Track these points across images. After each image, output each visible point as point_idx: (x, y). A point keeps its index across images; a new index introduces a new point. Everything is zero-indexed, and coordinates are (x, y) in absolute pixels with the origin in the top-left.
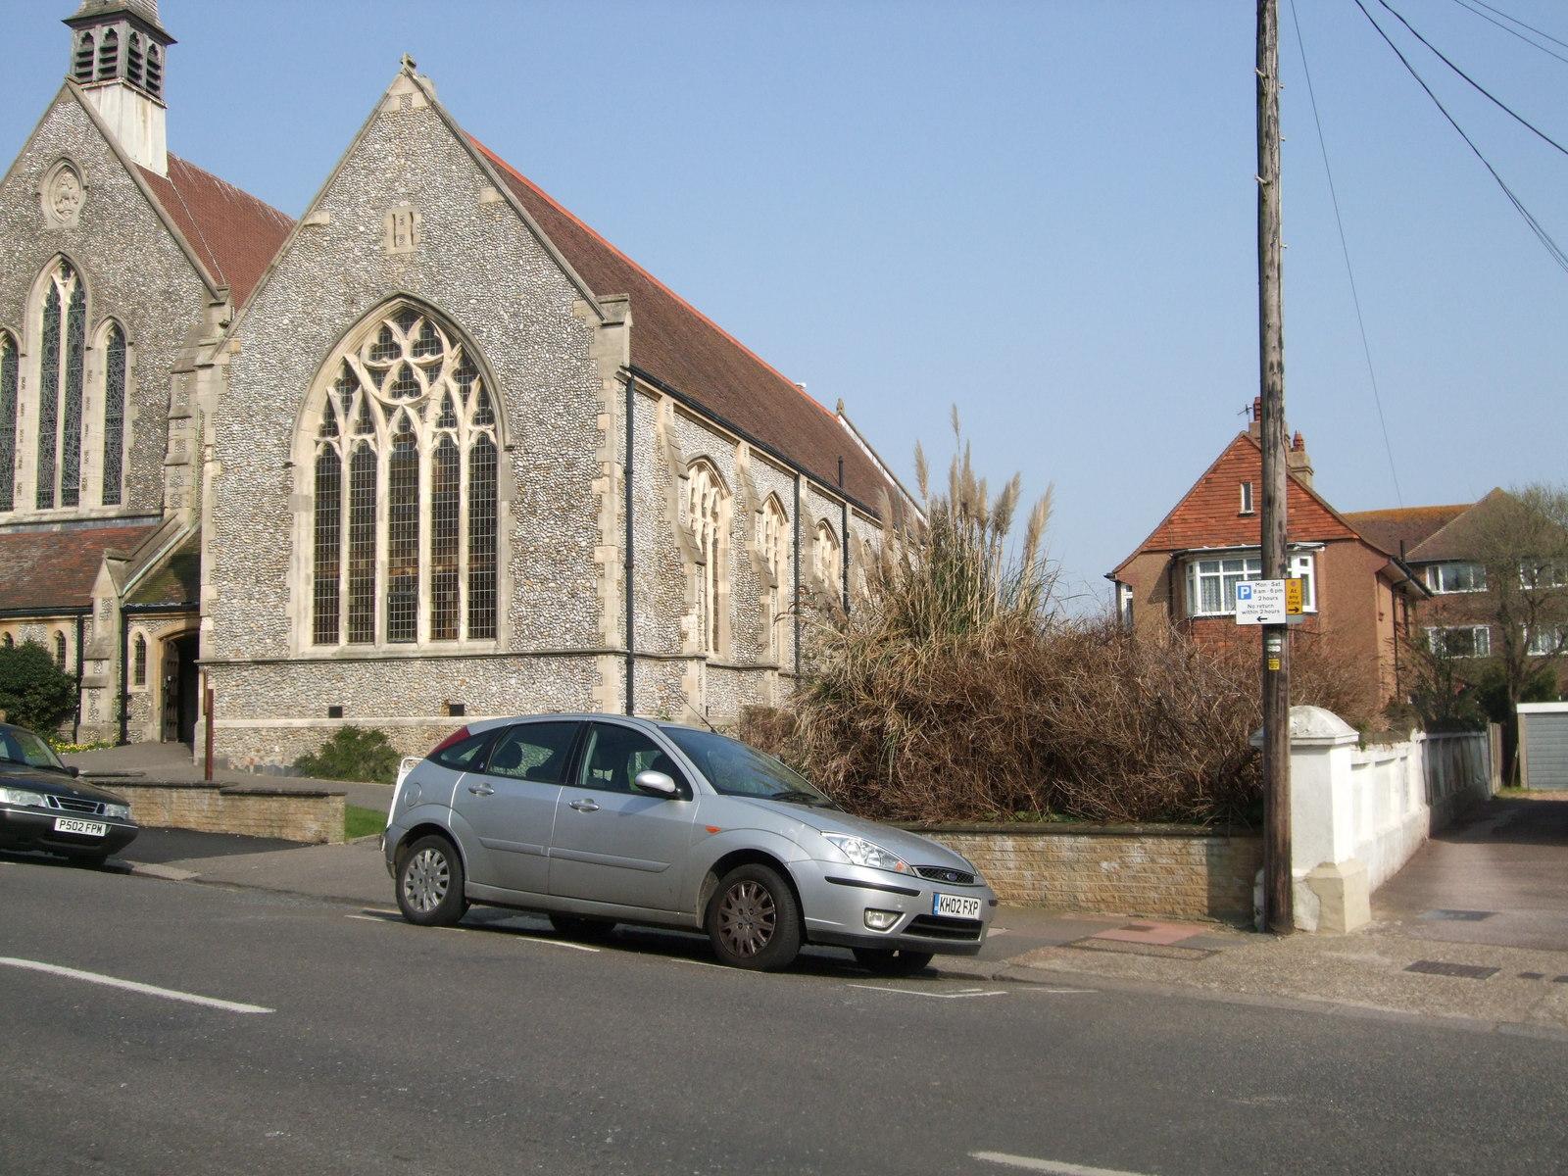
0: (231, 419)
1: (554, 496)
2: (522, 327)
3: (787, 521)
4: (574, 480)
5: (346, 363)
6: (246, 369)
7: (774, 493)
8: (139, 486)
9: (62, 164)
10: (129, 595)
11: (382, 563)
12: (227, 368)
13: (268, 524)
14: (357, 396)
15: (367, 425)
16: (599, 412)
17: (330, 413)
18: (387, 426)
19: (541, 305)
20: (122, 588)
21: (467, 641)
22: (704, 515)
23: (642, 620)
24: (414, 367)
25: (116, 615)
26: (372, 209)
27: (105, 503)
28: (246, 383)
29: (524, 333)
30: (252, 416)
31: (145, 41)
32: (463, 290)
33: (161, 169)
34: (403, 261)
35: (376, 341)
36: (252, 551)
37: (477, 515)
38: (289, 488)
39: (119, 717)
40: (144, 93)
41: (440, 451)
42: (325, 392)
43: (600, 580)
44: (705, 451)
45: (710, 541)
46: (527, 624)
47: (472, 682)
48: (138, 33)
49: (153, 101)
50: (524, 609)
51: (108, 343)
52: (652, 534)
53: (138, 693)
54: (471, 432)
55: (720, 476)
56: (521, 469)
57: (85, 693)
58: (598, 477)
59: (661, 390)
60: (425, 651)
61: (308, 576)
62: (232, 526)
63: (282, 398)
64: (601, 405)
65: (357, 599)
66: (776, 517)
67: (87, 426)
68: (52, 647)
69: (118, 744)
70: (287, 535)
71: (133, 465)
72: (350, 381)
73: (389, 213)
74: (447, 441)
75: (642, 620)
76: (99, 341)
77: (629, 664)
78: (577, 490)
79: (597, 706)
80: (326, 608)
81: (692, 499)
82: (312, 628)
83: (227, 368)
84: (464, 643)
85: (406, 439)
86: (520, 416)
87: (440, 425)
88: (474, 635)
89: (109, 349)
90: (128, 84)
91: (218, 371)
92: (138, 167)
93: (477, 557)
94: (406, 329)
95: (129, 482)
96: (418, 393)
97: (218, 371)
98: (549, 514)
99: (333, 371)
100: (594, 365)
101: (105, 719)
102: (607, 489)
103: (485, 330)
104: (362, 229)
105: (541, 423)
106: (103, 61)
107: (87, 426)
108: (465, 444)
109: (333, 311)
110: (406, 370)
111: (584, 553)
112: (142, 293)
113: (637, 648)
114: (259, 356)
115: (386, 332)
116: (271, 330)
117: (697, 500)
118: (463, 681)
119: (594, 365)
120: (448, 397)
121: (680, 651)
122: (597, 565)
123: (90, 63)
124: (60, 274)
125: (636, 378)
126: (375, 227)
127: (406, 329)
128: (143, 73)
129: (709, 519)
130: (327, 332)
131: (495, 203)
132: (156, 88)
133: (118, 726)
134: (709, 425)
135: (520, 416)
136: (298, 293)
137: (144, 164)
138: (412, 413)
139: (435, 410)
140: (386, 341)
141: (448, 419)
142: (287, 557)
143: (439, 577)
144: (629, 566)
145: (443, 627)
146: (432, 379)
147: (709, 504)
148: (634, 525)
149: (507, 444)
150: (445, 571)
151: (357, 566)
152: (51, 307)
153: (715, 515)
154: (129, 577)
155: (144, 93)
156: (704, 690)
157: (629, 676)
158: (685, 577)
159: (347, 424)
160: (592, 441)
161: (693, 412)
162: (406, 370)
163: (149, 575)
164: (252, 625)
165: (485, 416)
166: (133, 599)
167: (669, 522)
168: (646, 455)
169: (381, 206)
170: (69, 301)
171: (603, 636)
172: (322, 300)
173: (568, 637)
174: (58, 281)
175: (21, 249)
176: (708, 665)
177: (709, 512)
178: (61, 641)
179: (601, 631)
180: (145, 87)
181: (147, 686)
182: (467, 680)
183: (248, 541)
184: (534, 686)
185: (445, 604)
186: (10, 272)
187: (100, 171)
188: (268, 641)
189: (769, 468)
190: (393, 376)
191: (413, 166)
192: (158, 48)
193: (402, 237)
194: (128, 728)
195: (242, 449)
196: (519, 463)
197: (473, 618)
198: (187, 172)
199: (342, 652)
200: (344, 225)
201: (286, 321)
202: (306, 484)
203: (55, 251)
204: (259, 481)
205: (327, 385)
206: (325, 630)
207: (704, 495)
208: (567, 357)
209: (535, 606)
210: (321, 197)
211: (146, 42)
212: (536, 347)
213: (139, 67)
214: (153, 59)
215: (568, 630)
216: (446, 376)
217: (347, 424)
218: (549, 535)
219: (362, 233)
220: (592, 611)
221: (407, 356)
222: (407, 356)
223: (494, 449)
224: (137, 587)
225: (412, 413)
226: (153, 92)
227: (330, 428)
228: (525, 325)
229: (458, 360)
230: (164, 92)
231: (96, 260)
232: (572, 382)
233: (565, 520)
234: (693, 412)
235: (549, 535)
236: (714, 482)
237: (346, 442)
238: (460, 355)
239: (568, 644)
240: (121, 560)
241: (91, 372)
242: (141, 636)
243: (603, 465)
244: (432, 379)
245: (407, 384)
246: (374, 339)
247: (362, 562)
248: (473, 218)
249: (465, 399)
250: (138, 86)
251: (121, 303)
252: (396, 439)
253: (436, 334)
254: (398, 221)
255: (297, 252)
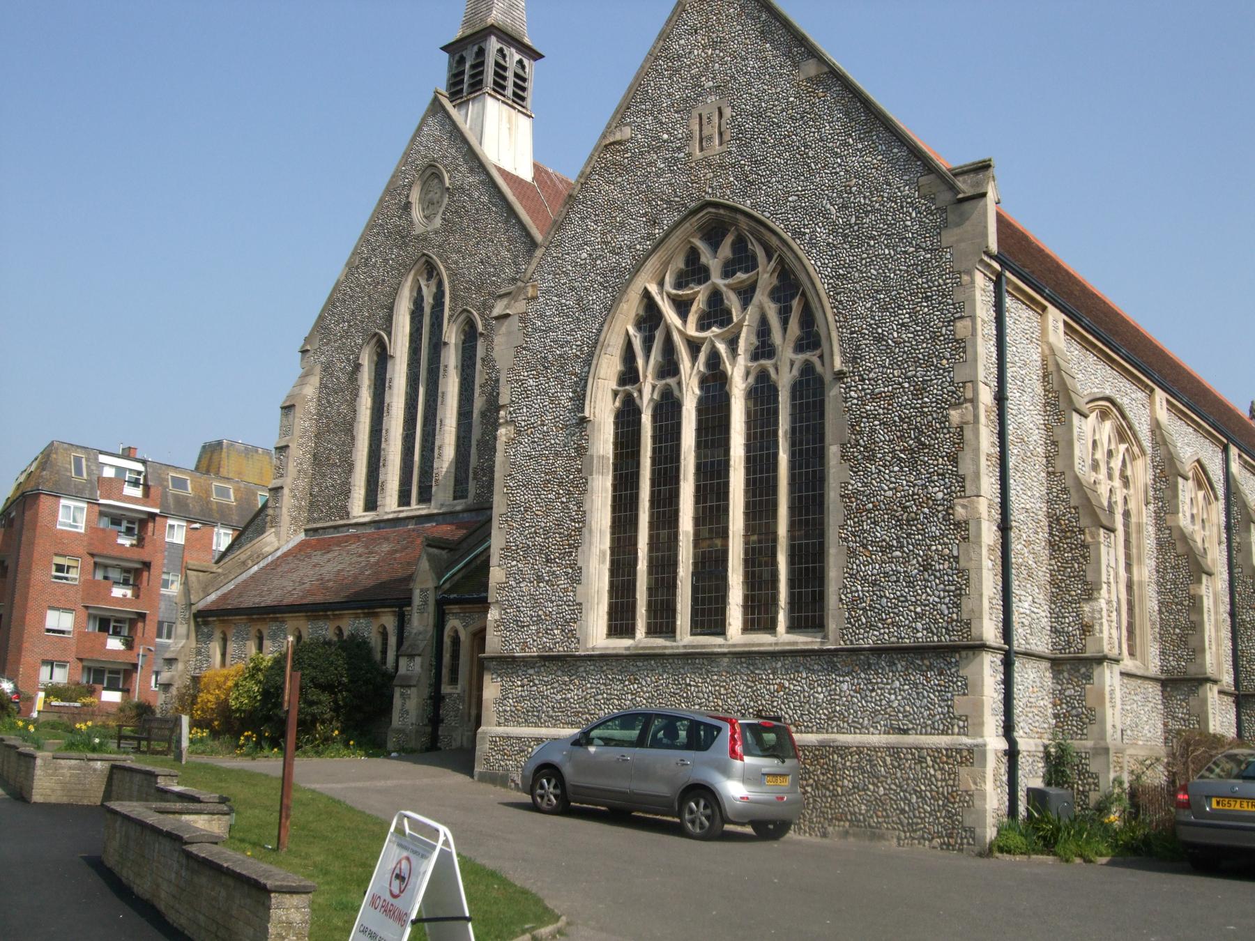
0: (526, 374)
1: (898, 434)
2: (853, 220)
3: (1216, 498)
4: (926, 410)
5: (647, 294)
6: (541, 316)
7: (1198, 461)
8: (484, 479)
9: (428, 172)
10: (447, 586)
11: (687, 533)
12: (523, 318)
13: (561, 492)
14: (659, 335)
15: (669, 368)
16: (957, 315)
17: (629, 355)
18: (693, 365)
19: (876, 190)
20: (439, 579)
21: (788, 632)
22: (1110, 477)
23: (1026, 605)
24: (724, 289)
25: (431, 608)
26: (676, 112)
27: (455, 498)
28: (541, 331)
29: (856, 228)
30: (546, 368)
31: (512, 55)
32: (780, 187)
33: (527, 174)
34: (710, 166)
35: (681, 265)
36: (543, 525)
37: (801, 468)
38: (584, 448)
39: (430, 720)
40: (510, 102)
41: (756, 389)
42: (624, 332)
43: (963, 545)
44: (1108, 392)
45: (1119, 511)
46: (864, 609)
47: (792, 687)
48: (504, 47)
49: (519, 111)
50: (859, 588)
51: (463, 337)
52: (1039, 490)
53: (450, 694)
54: (792, 363)
55: (1131, 428)
56: (855, 401)
57: (397, 692)
58: (957, 405)
59: (1046, 299)
60: (734, 646)
61: (604, 553)
62: (522, 497)
63: (579, 343)
64: (960, 306)
65: (657, 579)
66: (1201, 494)
67: (441, 421)
68: (375, 640)
69: (428, 750)
70: (580, 504)
71: (480, 458)
72: (650, 318)
73: (695, 113)
74: (763, 377)
75: (1026, 605)
76: (452, 335)
77: (1008, 664)
78: (929, 425)
79: (961, 723)
80: (623, 592)
81: (1093, 454)
82: (606, 617)
83: (523, 318)
84: (783, 636)
85: (715, 383)
86: (852, 333)
87: (755, 356)
88: (793, 627)
89: (463, 343)
90: (493, 93)
91: (514, 323)
92: (499, 169)
93: (800, 521)
94: (715, 245)
95: (475, 473)
96: (730, 320)
97: (514, 323)
98: (893, 458)
99: (630, 307)
100: (948, 256)
101: (414, 722)
102: (970, 418)
103: (807, 231)
104: (666, 136)
105: (879, 339)
106: (472, 76)
107: (441, 421)
108: (784, 380)
109: (634, 236)
110: (716, 298)
111: (940, 508)
112: (493, 283)
113: (1019, 643)
114: (556, 299)
115: (693, 256)
116: (570, 268)
117: (1100, 455)
118: (782, 686)
119: (948, 256)
120: (764, 322)
121: (1083, 650)
122: (957, 525)
123: (462, 81)
124: (426, 276)
125: (1008, 274)
126: (680, 132)
127: (715, 245)
128: (510, 84)
129: (1117, 483)
130: (627, 262)
131: (817, 76)
132: (523, 99)
133: (429, 729)
134: (1113, 360)
135: (852, 333)
136: (596, 222)
137: (509, 168)
138: (722, 348)
139: (745, 341)
140: (693, 264)
141: (763, 349)
142: (579, 530)
143: (754, 549)
144: (1004, 527)
145: (759, 617)
146: (746, 302)
147: (1116, 464)
148: (1011, 472)
149: (836, 370)
150: (760, 541)
151: (658, 538)
152: (417, 308)
153: (1126, 482)
154: (448, 568)
155: (510, 102)
156: (1119, 706)
157: (1008, 682)
158: (1087, 547)
159: (647, 368)
160: (948, 355)
161: (1091, 338)
162: (716, 298)
163: (473, 565)
164: (540, 613)
165: (810, 340)
166: (450, 591)
167: (1063, 473)
168: (1026, 381)
169: (685, 107)
170: (431, 300)
171: (968, 624)
172: (622, 224)
173: (919, 625)
174: (423, 283)
175: (393, 256)
176: (1122, 674)
177: (1117, 473)
178: (384, 634)
179: (965, 617)
180: (512, 97)
181: (459, 686)
182: (787, 684)
183: (539, 513)
184: (874, 694)
185: (760, 584)
186: (384, 280)
187: (461, 172)
188: (556, 632)
189: (1191, 430)
190: (699, 305)
191: (722, 54)
192: (526, 62)
193: (710, 138)
194: (440, 733)
195: (537, 406)
196: (853, 394)
197: (795, 603)
198: (557, 182)
199: (636, 648)
200: (646, 136)
201: (584, 255)
202: (604, 442)
203: (420, 254)
204: (553, 442)
205: (625, 323)
206: (620, 622)
207: (1110, 454)
208: (912, 249)
209: (874, 584)
210: (622, 111)
211: (514, 56)
212: (872, 243)
213: (504, 78)
214: (520, 72)
215: (919, 616)
216: (761, 297)
217: (647, 368)
218: (892, 486)
219: (665, 141)
220: (953, 588)
221: (717, 280)
222: (717, 280)
223: (820, 381)
224: (456, 578)
225: (722, 348)
226: (521, 102)
227: (629, 375)
228: (857, 218)
229: (776, 274)
230: (529, 103)
231: (455, 257)
232: (920, 281)
233: (913, 464)
234: (1091, 338)
235: (892, 486)
236: (1122, 437)
237: (647, 390)
238: (779, 268)
239: (920, 635)
240: (443, 549)
241: (446, 366)
242: (456, 632)
243: (964, 387)
244: (746, 302)
245: (716, 314)
246: (679, 263)
247: (664, 533)
248: (791, 99)
249: (785, 323)
250: (504, 96)
251: (474, 296)
252: (703, 382)
253: (750, 246)
254: (705, 120)
255: (597, 177)
